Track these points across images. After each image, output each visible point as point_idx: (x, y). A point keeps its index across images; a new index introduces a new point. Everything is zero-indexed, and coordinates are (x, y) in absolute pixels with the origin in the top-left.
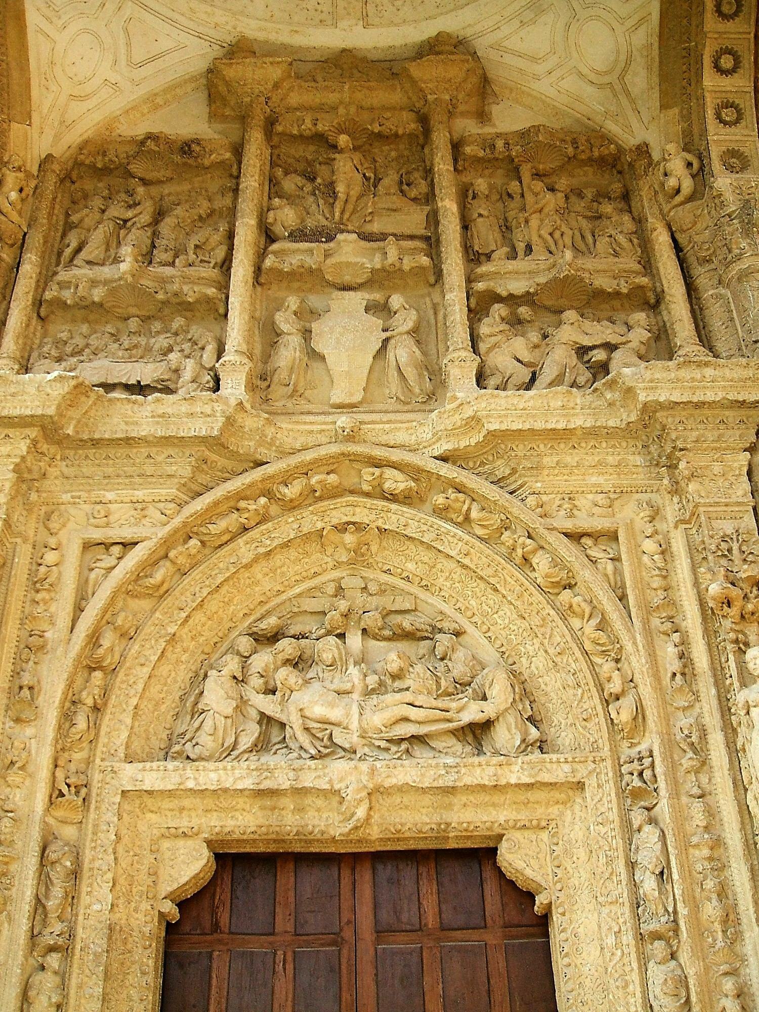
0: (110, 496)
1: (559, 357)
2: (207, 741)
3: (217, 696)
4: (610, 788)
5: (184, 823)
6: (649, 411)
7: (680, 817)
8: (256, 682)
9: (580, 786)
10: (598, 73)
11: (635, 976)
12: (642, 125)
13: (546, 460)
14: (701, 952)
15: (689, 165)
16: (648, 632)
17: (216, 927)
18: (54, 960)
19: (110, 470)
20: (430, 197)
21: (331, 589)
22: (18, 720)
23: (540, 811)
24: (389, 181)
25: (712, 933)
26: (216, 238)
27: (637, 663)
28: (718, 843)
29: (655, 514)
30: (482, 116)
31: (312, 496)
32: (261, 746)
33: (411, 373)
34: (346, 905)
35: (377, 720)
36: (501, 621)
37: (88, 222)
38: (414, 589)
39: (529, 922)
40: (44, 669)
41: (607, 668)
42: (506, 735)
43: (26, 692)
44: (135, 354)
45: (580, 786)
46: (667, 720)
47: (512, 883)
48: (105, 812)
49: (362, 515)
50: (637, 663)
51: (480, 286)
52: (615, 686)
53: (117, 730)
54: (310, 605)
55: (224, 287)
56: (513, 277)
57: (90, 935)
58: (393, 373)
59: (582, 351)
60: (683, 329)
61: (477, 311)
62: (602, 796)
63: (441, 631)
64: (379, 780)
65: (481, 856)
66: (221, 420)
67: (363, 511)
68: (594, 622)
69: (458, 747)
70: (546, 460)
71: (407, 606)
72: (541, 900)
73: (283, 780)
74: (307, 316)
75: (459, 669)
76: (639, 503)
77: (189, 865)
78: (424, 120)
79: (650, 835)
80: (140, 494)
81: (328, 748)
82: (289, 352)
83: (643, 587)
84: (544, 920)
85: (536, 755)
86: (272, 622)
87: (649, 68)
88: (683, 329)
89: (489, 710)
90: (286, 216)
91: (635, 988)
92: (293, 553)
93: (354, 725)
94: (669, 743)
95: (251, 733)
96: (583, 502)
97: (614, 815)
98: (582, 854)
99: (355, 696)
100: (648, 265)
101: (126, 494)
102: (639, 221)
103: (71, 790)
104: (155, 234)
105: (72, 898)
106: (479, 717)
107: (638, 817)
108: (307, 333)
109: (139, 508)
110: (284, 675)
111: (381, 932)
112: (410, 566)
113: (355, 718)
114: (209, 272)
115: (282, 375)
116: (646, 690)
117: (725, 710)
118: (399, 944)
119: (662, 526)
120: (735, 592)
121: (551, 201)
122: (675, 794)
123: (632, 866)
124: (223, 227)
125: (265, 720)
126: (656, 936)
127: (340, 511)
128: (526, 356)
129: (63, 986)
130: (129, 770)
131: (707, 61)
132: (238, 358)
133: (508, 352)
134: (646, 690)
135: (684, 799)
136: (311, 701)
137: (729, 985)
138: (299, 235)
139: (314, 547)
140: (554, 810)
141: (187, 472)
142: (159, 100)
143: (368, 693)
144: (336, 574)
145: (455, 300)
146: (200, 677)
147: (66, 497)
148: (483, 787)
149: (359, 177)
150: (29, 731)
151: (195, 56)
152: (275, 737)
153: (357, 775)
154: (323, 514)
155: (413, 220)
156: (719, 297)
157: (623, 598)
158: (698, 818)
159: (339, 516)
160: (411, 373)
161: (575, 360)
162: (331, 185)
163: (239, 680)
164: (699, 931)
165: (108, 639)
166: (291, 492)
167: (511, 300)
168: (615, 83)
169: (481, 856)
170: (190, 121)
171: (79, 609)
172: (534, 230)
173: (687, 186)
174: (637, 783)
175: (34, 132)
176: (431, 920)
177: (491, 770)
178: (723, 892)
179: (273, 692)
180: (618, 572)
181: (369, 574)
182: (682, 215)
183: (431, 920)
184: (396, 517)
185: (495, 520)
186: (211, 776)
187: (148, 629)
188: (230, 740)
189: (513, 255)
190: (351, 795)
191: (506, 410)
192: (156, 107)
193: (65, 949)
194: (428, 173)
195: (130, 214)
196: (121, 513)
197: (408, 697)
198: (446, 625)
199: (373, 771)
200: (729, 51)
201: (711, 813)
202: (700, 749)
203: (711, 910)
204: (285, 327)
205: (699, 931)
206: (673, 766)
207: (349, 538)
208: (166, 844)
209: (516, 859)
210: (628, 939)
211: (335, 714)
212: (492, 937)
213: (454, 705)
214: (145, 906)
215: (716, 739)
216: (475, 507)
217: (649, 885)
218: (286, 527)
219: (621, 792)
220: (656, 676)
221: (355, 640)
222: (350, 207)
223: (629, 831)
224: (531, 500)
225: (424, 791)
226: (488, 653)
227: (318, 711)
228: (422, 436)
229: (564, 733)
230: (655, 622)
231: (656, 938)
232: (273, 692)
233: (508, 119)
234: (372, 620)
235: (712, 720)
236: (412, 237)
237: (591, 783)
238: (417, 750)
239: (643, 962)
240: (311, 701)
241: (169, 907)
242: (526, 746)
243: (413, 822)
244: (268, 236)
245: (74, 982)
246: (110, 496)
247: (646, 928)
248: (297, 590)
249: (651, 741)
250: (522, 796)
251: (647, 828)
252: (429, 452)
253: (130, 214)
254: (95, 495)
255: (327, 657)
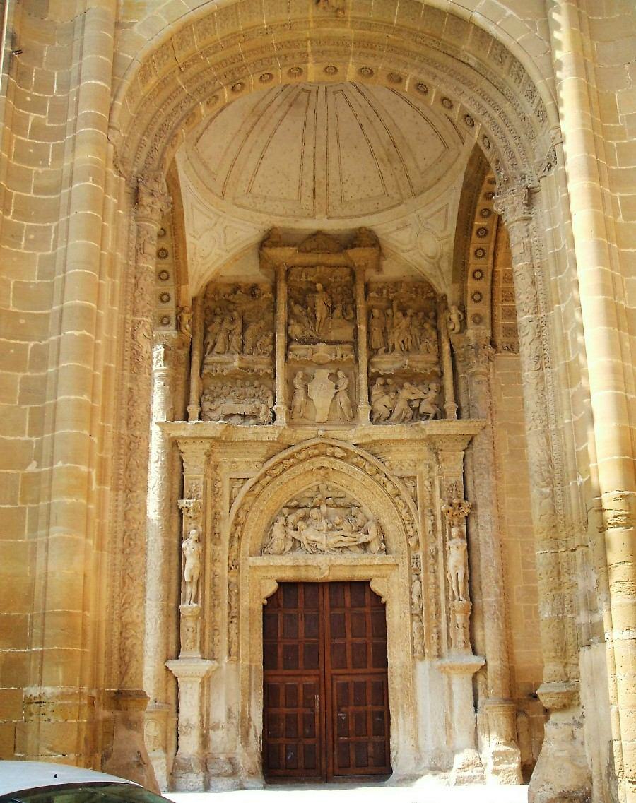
0: (237, 459)
1: (401, 405)
2: (276, 548)
3: (278, 531)
4: (406, 567)
5: (269, 575)
6: (430, 437)
7: (427, 579)
8: (291, 526)
9: (397, 565)
10: (429, 257)
11: (409, 626)
12: (445, 286)
13: (393, 448)
14: (428, 621)
15: (459, 316)
16: (423, 516)
17: (279, 606)
18: (235, 620)
19: (237, 451)
20: (354, 320)
21: (315, 489)
22: (215, 544)
23: (384, 572)
24: (338, 312)
25: (432, 615)
26: (268, 340)
27: (418, 526)
28: (438, 587)
29: (430, 467)
30: (379, 269)
31: (309, 457)
32: (293, 549)
33: (345, 408)
34: (321, 600)
35: (332, 541)
36: (374, 503)
37: (216, 331)
38: (344, 489)
39: (379, 606)
40: (222, 526)
41: (408, 527)
42: (374, 547)
43: (217, 535)
44: (241, 398)
45: (397, 565)
46: (426, 546)
47: (375, 594)
48: (245, 572)
49: (326, 464)
50: (418, 526)
51: (373, 370)
52: (410, 533)
53: (247, 545)
54: (308, 495)
55: (273, 363)
56: (386, 363)
57: (244, 613)
58: (338, 407)
59: (410, 401)
60: (450, 405)
61: (372, 381)
62: (404, 570)
63: (354, 506)
64: (332, 563)
65: (365, 584)
66: (277, 435)
67: (327, 462)
68: (406, 510)
69: (358, 550)
70: (393, 448)
71: (342, 496)
72: (383, 600)
73: (302, 563)
74: (307, 379)
75: (359, 522)
76: (425, 464)
77: (271, 588)
78: (353, 274)
79: (417, 584)
80: (248, 459)
81: (315, 549)
82: (299, 400)
83: (423, 498)
84: (384, 605)
85: (383, 555)
86: (295, 503)
87: (449, 261)
88: (450, 405)
89: (369, 538)
90: (296, 330)
91: (409, 629)
92: (302, 477)
93: (324, 542)
94: (425, 554)
95: (290, 545)
96: (406, 464)
97: (407, 576)
98: (396, 587)
99: (324, 532)
100: (439, 362)
101: (244, 459)
102: (438, 333)
103: (234, 566)
104: (244, 338)
105: (238, 601)
106: (366, 541)
107: (414, 577)
108: (306, 388)
109: (247, 465)
110: (300, 525)
111: (332, 607)
112: (343, 481)
113: (323, 540)
114: (266, 359)
115: (297, 409)
116: (420, 534)
117: (444, 545)
118: (337, 611)
119: (432, 474)
120: (450, 509)
121: (404, 323)
122: (426, 569)
123: (411, 593)
124: (271, 335)
125: (293, 539)
126: (417, 615)
127: (318, 462)
128: (388, 405)
129: (238, 627)
130: (251, 559)
131: (470, 274)
132: (281, 406)
133: (382, 403)
134: (420, 534)
135: (429, 573)
136: (309, 534)
137: (435, 630)
138: (302, 342)
139: (310, 476)
140: (389, 572)
141: (265, 451)
142: (237, 257)
143: (329, 530)
144: (317, 483)
145: (363, 377)
146: (272, 524)
147: (221, 460)
148: (366, 565)
149: (325, 307)
150: (219, 548)
151: (250, 233)
152: (298, 545)
153: (326, 565)
154: (313, 464)
155: (345, 333)
156: (464, 378)
157: (415, 502)
158: (432, 580)
159: (318, 464)
160: (345, 408)
161: (407, 407)
162: (314, 312)
163: (285, 526)
164: (428, 614)
165: (242, 515)
166: (301, 457)
167: (385, 376)
168: (436, 261)
169: (365, 584)
170: (251, 272)
171: (231, 504)
172: (395, 338)
173: (457, 328)
174: (415, 567)
175: (189, 287)
176: (348, 604)
177: (368, 560)
178: (437, 603)
179: (297, 529)
180: (415, 490)
181: (329, 483)
182: (455, 339)
183: (348, 604)
184: (339, 464)
185: (374, 469)
186: (278, 561)
187: (254, 509)
188: (283, 548)
189: (386, 351)
190: (324, 568)
191: (381, 432)
192: (236, 260)
193: (238, 617)
194: (355, 310)
195: (232, 327)
196: (243, 466)
197: (342, 533)
198: (356, 504)
199: (331, 559)
200: (482, 275)
201: (436, 578)
202: (435, 558)
203: (433, 608)
204: (297, 387)
205: (428, 614)
206: (426, 562)
207: (322, 472)
208: (263, 581)
209: (375, 586)
210: (408, 615)
211: (317, 539)
212: (367, 610)
213: (357, 536)
214: (258, 602)
215: (441, 554)
216: (367, 464)
217: (415, 600)
218: (300, 468)
219: (410, 568)
220: (424, 532)
221: (323, 508)
222: (322, 324)
223: (411, 582)
224: (387, 464)
225: (347, 566)
226: (370, 515)
227: (312, 538)
228: (351, 436)
229: (393, 545)
230: (426, 511)
231: (416, 616)
232: (297, 529)
233: (391, 271)
234: (330, 501)
235: (440, 548)
236: (347, 342)
237: (401, 565)
238: (345, 551)
239: (412, 621)
240: (309, 534)
241: (265, 602)
242: (381, 550)
243: (343, 575)
244: (289, 340)
245: (241, 625)
246: (237, 459)
247: (414, 612)
248: (303, 489)
249: (420, 553)
250: (378, 568)
251: (417, 581)
252: (351, 442)
253: (232, 327)
254: (232, 459)
255: (315, 516)
